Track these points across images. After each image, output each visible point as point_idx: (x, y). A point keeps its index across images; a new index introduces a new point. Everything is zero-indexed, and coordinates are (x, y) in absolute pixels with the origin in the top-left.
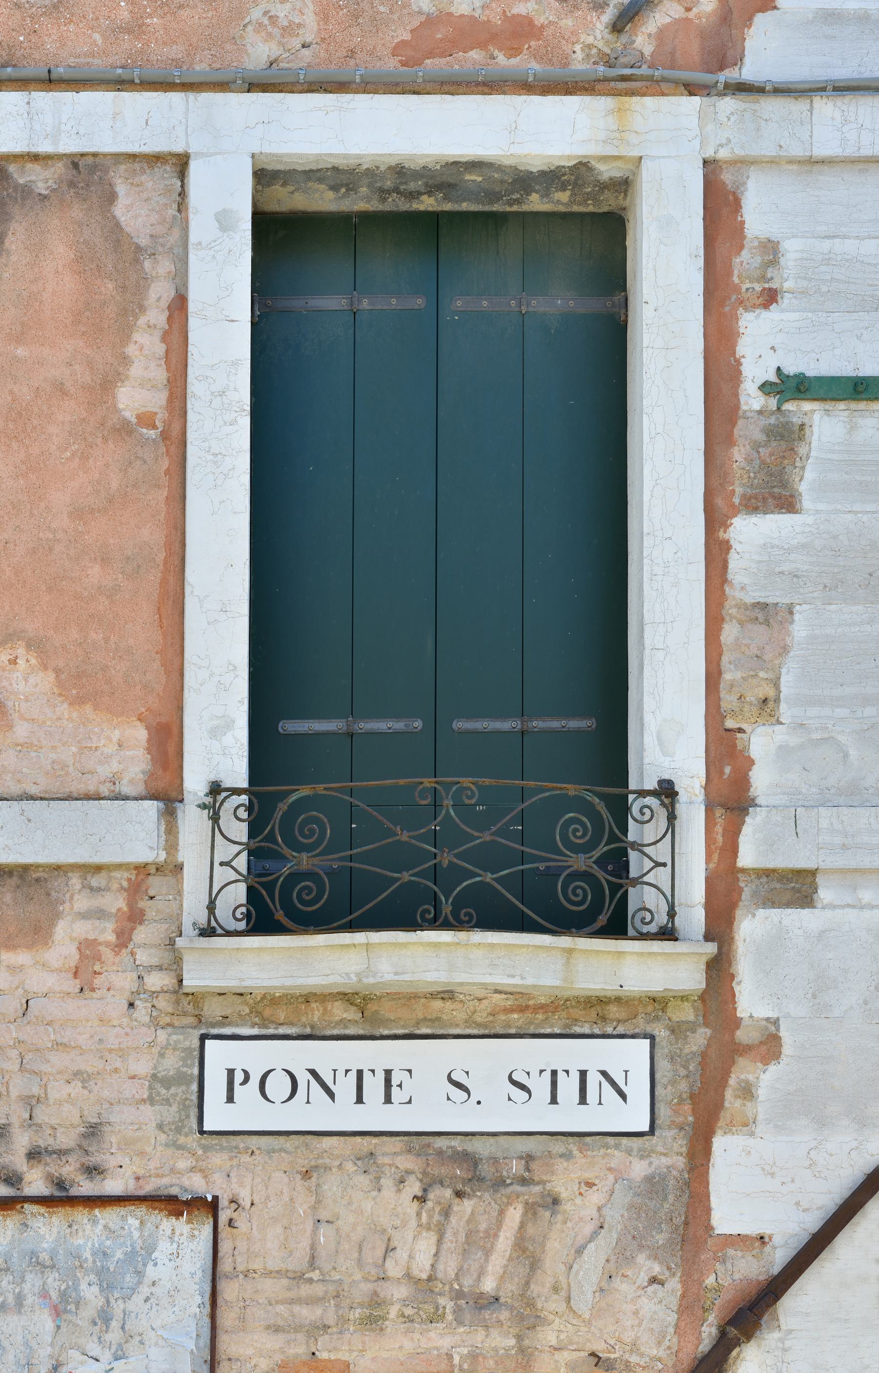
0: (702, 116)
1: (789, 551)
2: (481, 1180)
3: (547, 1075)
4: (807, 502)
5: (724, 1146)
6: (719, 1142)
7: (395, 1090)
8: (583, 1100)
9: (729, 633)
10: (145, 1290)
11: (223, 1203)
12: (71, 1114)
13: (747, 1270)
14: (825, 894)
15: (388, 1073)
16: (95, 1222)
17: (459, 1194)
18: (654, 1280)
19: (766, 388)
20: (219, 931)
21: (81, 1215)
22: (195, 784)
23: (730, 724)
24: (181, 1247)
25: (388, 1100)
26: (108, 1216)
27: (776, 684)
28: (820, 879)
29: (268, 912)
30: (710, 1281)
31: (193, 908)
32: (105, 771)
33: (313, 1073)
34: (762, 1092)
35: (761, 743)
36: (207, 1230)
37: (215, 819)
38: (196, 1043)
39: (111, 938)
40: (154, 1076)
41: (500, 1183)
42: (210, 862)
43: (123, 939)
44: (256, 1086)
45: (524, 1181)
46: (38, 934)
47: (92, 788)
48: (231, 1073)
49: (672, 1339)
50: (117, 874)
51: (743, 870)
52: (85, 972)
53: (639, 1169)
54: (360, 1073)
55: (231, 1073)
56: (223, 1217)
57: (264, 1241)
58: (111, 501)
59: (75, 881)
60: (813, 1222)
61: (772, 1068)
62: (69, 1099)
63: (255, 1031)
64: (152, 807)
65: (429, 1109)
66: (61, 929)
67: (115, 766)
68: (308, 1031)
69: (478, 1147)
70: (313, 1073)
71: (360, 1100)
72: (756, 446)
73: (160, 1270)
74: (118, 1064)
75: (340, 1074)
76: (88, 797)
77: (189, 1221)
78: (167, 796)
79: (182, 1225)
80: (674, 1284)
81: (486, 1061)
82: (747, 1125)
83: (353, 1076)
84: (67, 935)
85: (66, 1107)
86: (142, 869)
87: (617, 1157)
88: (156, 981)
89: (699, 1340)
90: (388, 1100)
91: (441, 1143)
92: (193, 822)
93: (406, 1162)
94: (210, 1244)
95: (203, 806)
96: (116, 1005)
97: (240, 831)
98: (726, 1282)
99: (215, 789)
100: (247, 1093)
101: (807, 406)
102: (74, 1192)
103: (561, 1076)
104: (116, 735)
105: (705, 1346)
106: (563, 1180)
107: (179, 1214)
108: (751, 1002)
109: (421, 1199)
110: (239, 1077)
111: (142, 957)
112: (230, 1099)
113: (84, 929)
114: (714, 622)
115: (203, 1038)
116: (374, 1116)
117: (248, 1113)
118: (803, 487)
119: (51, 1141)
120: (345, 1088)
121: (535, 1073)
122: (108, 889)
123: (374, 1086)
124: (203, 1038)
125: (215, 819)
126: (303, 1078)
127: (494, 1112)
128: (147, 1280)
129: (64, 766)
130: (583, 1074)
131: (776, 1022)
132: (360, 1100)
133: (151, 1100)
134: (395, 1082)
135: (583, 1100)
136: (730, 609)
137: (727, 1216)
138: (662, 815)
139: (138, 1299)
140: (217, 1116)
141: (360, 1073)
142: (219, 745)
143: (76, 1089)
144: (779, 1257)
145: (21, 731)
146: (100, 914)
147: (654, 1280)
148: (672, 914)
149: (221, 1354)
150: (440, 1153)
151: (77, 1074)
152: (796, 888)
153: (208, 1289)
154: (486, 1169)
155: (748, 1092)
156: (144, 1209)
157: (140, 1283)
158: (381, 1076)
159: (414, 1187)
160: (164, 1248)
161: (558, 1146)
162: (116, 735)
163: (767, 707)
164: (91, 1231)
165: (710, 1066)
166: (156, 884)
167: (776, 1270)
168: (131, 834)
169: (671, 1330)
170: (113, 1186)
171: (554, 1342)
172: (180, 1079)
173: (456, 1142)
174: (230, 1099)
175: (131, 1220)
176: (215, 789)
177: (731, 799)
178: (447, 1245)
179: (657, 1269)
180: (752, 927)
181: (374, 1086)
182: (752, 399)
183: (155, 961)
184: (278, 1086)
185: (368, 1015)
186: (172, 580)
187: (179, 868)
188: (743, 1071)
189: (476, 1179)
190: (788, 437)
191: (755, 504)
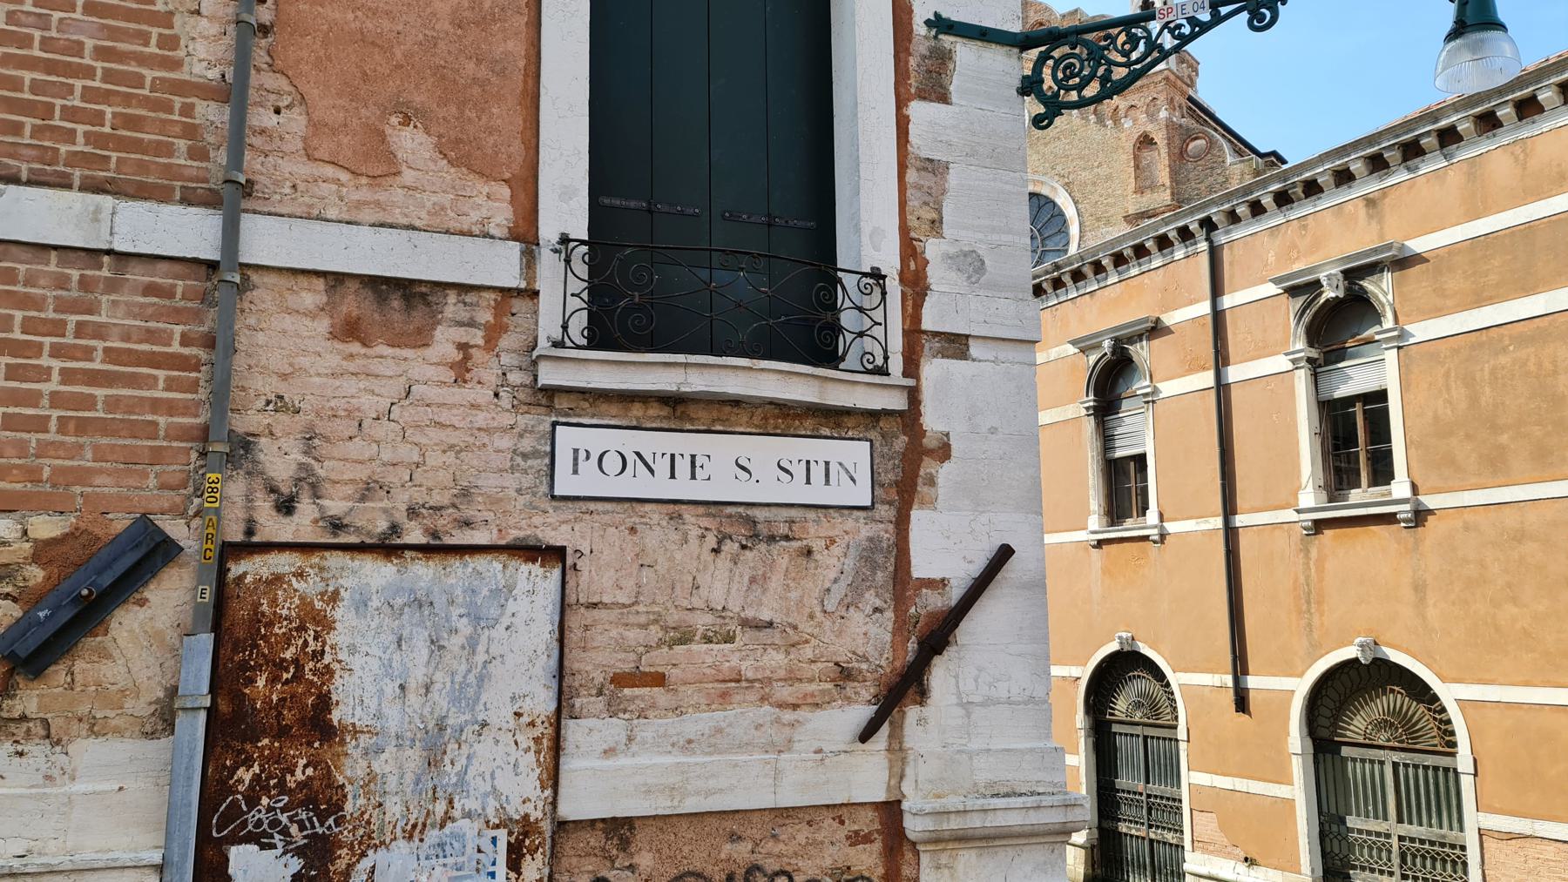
0: (1106, 571)
1: (945, 128)
2: (757, 536)
3: (803, 464)
4: (954, 98)
5: (917, 515)
6: (915, 514)
7: (698, 470)
8: (827, 482)
9: (912, 176)
10: (505, 621)
11: (569, 551)
12: (444, 477)
13: (934, 602)
14: (975, 349)
15: (693, 457)
16: (465, 566)
17: (744, 547)
18: (876, 610)
19: (928, 23)
20: (569, 343)
21: (455, 563)
22: (549, 232)
23: (913, 234)
24: (536, 587)
25: (693, 477)
26: (480, 562)
27: (940, 213)
28: (971, 342)
29: (602, 335)
30: (913, 610)
31: (549, 327)
32: (475, 216)
33: (638, 454)
34: (940, 480)
35: (933, 249)
36: (557, 572)
37: (568, 261)
38: (548, 428)
39: (481, 342)
40: (514, 451)
41: (772, 539)
42: (560, 297)
43: (491, 343)
44: (594, 458)
45: (787, 538)
46: (421, 339)
47: (465, 228)
48: (576, 451)
49: (888, 654)
50: (485, 295)
51: (925, 332)
52: (462, 370)
53: (866, 531)
54: (673, 456)
55: (576, 451)
56: (569, 562)
57: (594, 579)
58: (484, 18)
59: (452, 297)
60: (977, 568)
61: (946, 464)
62: (445, 466)
63: (595, 421)
64: (515, 248)
65: (721, 485)
66: (440, 333)
67: (485, 213)
68: (634, 423)
69: (760, 514)
70: (638, 454)
71: (673, 476)
72: (924, 57)
73: (519, 606)
74: (486, 440)
75: (658, 456)
76: (462, 233)
77: (542, 566)
78: (525, 234)
79: (536, 569)
80: (889, 614)
81: (765, 451)
82: (931, 503)
83: (668, 457)
84: (445, 341)
85: (441, 473)
86: (505, 292)
87: (850, 524)
88: (515, 378)
89: (906, 652)
90: (693, 477)
91: (729, 510)
92: (549, 267)
93: (705, 522)
94: (559, 583)
95: (556, 251)
96: (484, 395)
97: (582, 270)
98: (923, 612)
99: (565, 240)
100: (588, 467)
101: (952, 39)
102: (448, 540)
103: (813, 464)
104: (486, 190)
105: (910, 657)
106: (814, 532)
107: (534, 561)
108: (932, 421)
109: (716, 551)
110: (582, 455)
111: (506, 359)
112: (575, 472)
113: (462, 335)
114: (902, 168)
115: (554, 424)
116: (683, 488)
117: (588, 482)
118: (951, 88)
119: (427, 498)
120: (662, 466)
121: (795, 462)
122: (477, 305)
123: (683, 466)
124: (554, 424)
125: (568, 261)
126: (631, 458)
127: (767, 488)
128: (509, 612)
129: (443, 208)
130: (827, 463)
131: (947, 435)
132: (673, 476)
133: (513, 469)
134: (698, 464)
135: (827, 482)
136: (911, 160)
137: (921, 568)
138: (877, 291)
139: (501, 628)
140: (565, 484)
141: (673, 456)
142: (566, 207)
143: (450, 457)
144: (955, 594)
145: (408, 176)
146: (471, 324)
147: (876, 610)
148: (886, 358)
149: (567, 671)
150: (730, 516)
151: (452, 447)
152: (956, 345)
153: (557, 618)
154: (763, 529)
155: (931, 481)
156: (973, 853)
157: (502, 614)
158: (688, 459)
159: (711, 541)
160: (522, 585)
161: (811, 515)
162: (486, 190)
163: (936, 225)
164: (459, 571)
165: (908, 457)
166: (518, 305)
167: (953, 603)
168: (500, 265)
169: (888, 646)
170: (480, 537)
171: (811, 656)
172: (535, 454)
173: (741, 510)
174: (575, 472)
175: (491, 566)
176: (565, 240)
177: (916, 285)
178: (735, 587)
179: (878, 603)
180: (933, 370)
181: (683, 466)
182: (920, 29)
183: (516, 363)
184: (613, 464)
185: (677, 409)
186: (530, 82)
187: (537, 293)
188: (928, 466)
189: (755, 536)
190: (942, 58)
191: (923, 96)
